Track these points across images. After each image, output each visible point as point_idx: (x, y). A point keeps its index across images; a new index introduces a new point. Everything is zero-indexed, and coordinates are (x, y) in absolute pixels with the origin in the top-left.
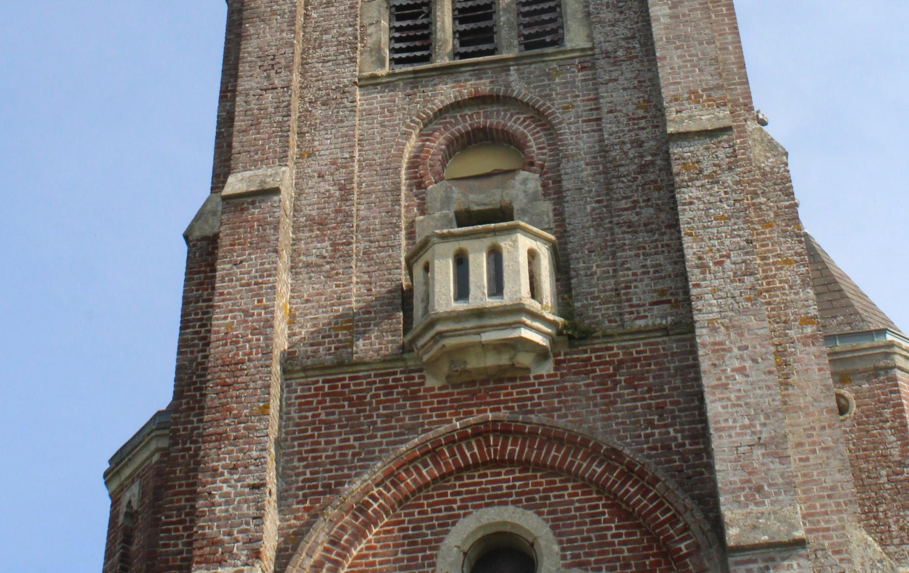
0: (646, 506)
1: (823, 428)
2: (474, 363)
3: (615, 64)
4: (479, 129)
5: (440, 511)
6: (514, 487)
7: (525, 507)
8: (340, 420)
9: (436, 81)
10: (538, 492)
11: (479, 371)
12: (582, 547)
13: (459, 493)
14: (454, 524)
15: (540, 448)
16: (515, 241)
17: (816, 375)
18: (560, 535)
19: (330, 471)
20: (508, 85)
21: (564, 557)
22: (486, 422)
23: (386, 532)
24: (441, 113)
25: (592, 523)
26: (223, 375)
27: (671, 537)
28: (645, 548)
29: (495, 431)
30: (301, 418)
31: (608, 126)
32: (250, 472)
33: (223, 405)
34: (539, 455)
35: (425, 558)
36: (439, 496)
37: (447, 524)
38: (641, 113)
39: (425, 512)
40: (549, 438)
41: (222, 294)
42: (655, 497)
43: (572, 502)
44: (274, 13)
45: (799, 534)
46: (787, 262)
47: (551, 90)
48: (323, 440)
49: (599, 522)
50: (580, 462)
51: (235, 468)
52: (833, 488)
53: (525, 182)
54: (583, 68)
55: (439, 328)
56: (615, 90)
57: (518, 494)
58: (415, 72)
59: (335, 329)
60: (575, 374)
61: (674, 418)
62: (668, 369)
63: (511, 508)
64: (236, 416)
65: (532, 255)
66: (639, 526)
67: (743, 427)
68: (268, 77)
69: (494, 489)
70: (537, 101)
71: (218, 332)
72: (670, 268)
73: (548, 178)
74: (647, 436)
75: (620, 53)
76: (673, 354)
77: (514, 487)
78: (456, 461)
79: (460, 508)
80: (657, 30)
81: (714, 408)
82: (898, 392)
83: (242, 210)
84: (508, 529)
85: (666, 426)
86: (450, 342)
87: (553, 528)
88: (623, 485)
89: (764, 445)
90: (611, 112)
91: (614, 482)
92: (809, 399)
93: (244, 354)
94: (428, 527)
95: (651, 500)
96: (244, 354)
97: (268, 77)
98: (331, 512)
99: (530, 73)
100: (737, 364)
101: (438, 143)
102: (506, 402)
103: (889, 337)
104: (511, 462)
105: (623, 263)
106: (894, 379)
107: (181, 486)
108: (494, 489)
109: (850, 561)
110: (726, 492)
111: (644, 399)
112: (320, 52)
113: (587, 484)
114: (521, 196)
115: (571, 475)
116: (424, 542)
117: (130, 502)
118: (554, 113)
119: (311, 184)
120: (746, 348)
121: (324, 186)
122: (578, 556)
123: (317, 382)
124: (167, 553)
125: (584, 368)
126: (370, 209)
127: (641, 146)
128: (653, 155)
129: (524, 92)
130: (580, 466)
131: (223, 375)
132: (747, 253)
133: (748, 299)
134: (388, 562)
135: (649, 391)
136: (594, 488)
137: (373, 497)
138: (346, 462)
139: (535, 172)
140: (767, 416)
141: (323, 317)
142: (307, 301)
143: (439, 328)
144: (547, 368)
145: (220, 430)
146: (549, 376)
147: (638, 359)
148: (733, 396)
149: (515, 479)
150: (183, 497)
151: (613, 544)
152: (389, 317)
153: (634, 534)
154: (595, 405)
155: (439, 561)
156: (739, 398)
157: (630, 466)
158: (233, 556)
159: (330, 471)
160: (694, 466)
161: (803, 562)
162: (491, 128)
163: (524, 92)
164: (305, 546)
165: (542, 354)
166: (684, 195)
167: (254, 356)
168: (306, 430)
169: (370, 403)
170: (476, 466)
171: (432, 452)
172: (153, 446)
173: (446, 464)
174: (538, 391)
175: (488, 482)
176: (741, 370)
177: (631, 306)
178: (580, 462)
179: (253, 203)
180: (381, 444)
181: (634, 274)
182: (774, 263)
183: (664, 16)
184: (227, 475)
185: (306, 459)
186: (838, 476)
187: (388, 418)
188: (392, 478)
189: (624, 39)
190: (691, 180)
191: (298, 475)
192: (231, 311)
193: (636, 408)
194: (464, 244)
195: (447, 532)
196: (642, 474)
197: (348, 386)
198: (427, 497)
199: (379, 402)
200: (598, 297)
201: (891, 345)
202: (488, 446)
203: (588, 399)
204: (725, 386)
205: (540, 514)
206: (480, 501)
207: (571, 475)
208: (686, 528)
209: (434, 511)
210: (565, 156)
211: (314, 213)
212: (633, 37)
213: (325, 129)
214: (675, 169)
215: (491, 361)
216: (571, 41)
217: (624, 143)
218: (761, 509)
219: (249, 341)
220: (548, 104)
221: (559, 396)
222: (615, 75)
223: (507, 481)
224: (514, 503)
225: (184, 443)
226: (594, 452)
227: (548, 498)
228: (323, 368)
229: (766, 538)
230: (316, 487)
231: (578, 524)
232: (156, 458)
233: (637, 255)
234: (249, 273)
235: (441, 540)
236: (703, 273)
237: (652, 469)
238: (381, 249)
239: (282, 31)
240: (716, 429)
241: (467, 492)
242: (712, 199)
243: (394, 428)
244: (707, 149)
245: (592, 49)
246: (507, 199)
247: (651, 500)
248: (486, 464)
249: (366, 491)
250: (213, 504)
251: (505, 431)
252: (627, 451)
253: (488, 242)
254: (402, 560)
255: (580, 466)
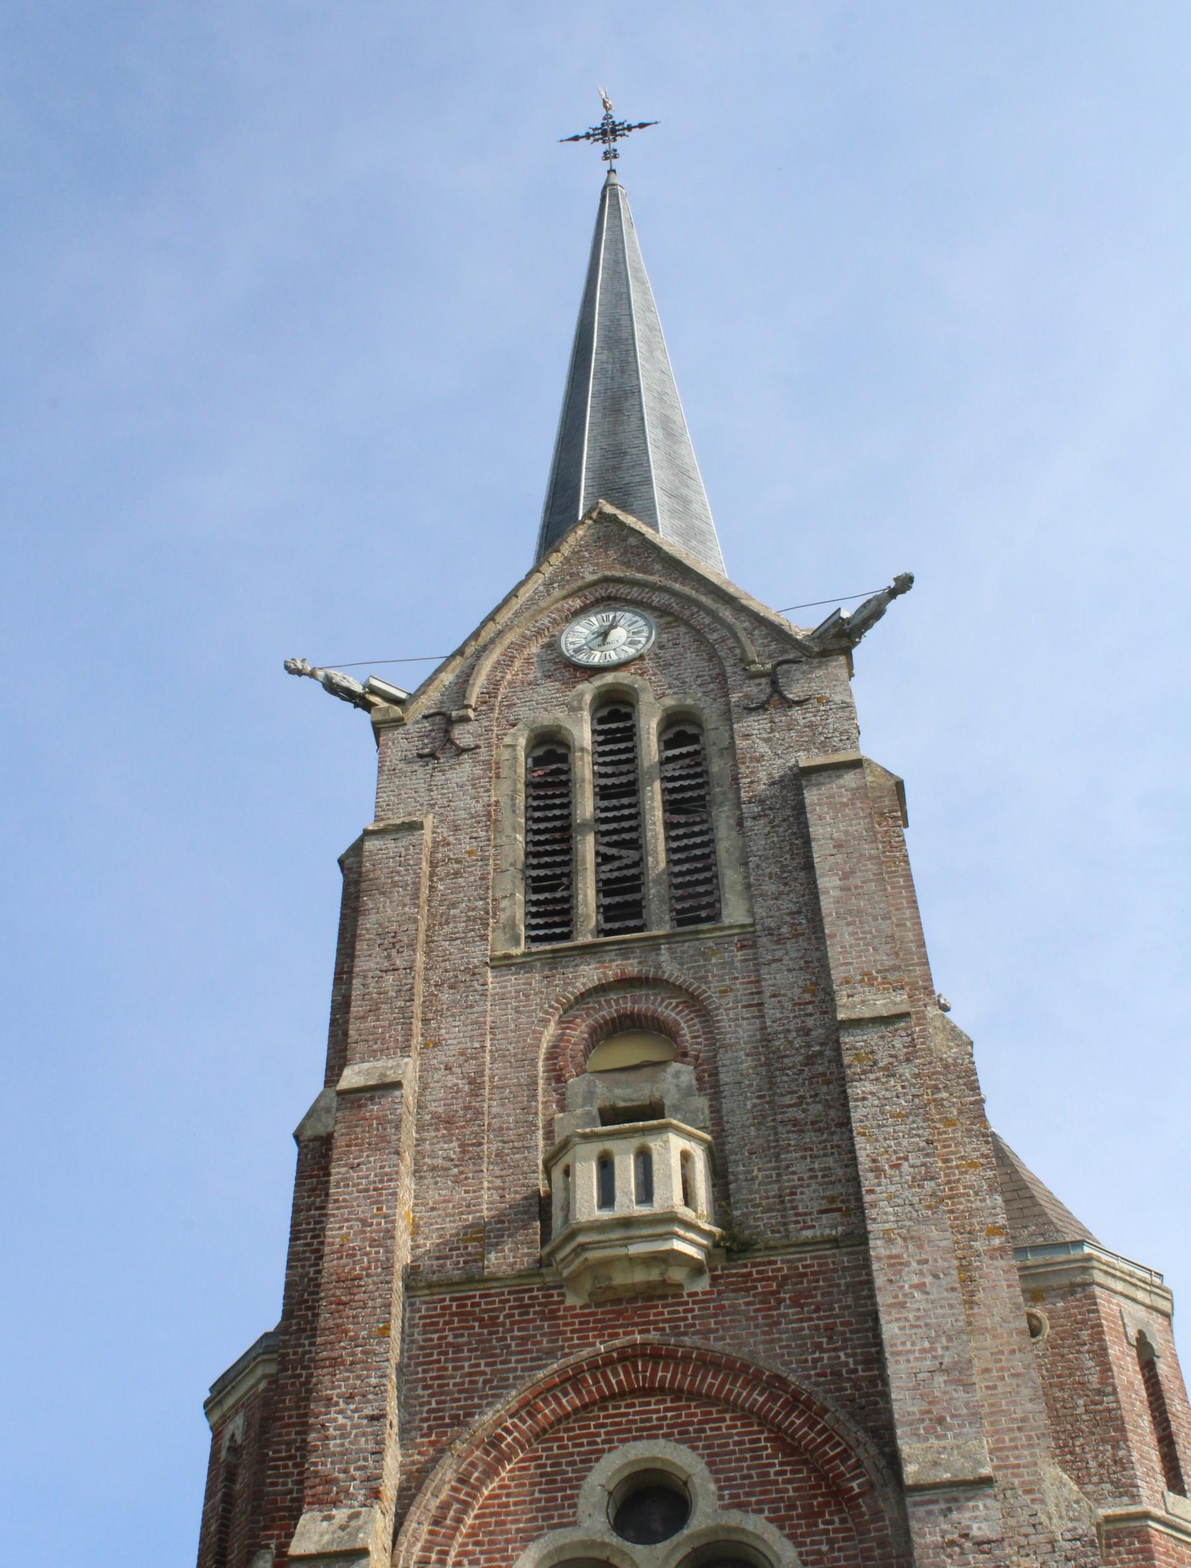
0: (813, 1440)
1: (1013, 1352)
2: (620, 1278)
3: (778, 942)
4: (625, 1016)
5: (582, 1445)
6: (665, 1418)
7: (678, 1441)
8: (469, 1343)
9: (578, 961)
10: (692, 1423)
11: (626, 1288)
12: (741, 1486)
13: (603, 1425)
14: (597, 1460)
15: (694, 1375)
16: (667, 1142)
17: (1005, 1293)
18: (717, 1472)
19: (459, 1400)
20: (658, 966)
21: (721, 1498)
22: (633, 1346)
23: (521, 1469)
24: (583, 997)
25: (753, 1458)
26: (338, 1292)
27: (842, 1474)
28: (812, 1487)
29: (643, 1355)
30: (425, 1340)
31: (771, 1012)
32: (369, 1401)
33: (338, 1326)
34: (692, 1382)
35: (564, 1498)
36: (580, 1428)
37: (590, 1460)
38: (808, 997)
39: (566, 1447)
40: (704, 1363)
41: (336, 1201)
42: (824, 1430)
43: (730, 1436)
44: (395, 884)
45: (986, 1471)
46: (973, 1165)
47: (708, 971)
48: (450, 1365)
49: (760, 1457)
50: (738, 1390)
51: (352, 1396)
52: (1023, 1420)
53: (677, 1075)
54: (743, 947)
55: (581, 1239)
56: (779, 971)
57: (669, 1426)
58: (553, 951)
59: (464, 1241)
60: (733, 1291)
61: (845, 1340)
62: (838, 1285)
63: (662, 1442)
64: (352, 1339)
65: (686, 1157)
66: (805, 1462)
67: (923, 1351)
68: (389, 957)
69: (642, 1421)
70: (691, 984)
71: (332, 1244)
72: (840, 1172)
73: (704, 1071)
74: (815, 1361)
75: (785, 930)
76: (844, 1269)
77: (665, 1418)
78: (599, 1389)
79: (604, 1442)
80: (827, 904)
81: (890, 1329)
82: (1097, 1311)
83: (360, 1106)
84: (659, 1465)
85: (836, 1349)
86: (594, 1255)
87: (709, 1464)
88: (787, 1415)
89: (946, 1371)
90: (774, 996)
91: (778, 1413)
92: (997, 1319)
93: (362, 1269)
94: (569, 1464)
95: (819, 1433)
96: (362, 1269)
97: (389, 957)
98: (459, 1446)
99: (683, 952)
100: (916, 1280)
101: (580, 1031)
102: (656, 1322)
103: (1087, 1250)
104: (662, 1389)
105: (788, 1167)
106: (1093, 1297)
107: (290, 1417)
108: (642, 1421)
109: (1042, 1501)
110: (904, 1424)
111: (811, 1319)
112: (446, 929)
113: (747, 1415)
114: (673, 1090)
115: (730, 1405)
116: (564, 1481)
117: (233, 1435)
118: (710, 997)
119: (436, 1077)
120: (926, 1261)
121: (451, 1080)
122: (737, 1496)
123: (444, 1300)
124: (275, 1493)
125: (744, 1285)
126: (503, 1105)
127: (807, 1034)
128: (821, 1044)
129: (676, 973)
130: (739, 1394)
131: (338, 1292)
132: (927, 1155)
133: (929, 1207)
134: (524, 1502)
135: (817, 1310)
136: (754, 1420)
137: (506, 1430)
138: (476, 1390)
139: (689, 1064)
140: (950, 1339)
141: (451, 1227)
142: (433, 1209)
143: (581, 1239)
144: (703, 1285)
145: (335, 1354)
146: (704, 1293)
147: (805, 1275)
148: (911, 1316)
149: (667, 1410)
150: (293, 1430)
151: (776, 1482)
152: (525, 1227)
153: (800, 1471)
154: (756, 1326)
155: (581, 1502)
156: (918, 1318)
157: (796, 1395)
158: (349, 1495)
159: (459, 1400)
160: (867, 1395)
161: (990, 1502)
162: (639, 1015)
163: (676, 973)
164: (430, 1485)
165: (697, 1269)
166: (856, 1090)
167: (372, 1271)
168: (431, 1355)
169: (504, 1324)
170: (622, 1394)
171: (572, 1379)
172: (259, 1372)
173: (589, 1392)
174: (692, 1310)
175: (636, 1413)
176: (921, 1287)
177: (797, 1215)
178: (738, 1390)
179: (372, 1099)
180: (515, 1369)
181: (801, 1179)
182: (958, 1167)
183: (834, 888)
184: (342, 1405)
185: (431, 1387)
186: (1029, 1406)
187: (523, 1340)
188: (528, 1408)
189: (789, 914)
190: (864, 1072)
191: (422, 1404)
192: (347, 1220)
193: (802, 1329)
194: (609, 1145)
195: (590, 1469)
196: (809, 1404)
197: (478, 1304)
198: (567, 1430)
199: (513, 1323)
200: (760, 1205)
201: (1089, 1258)
202: (636, 1372)
203: (748, 1319)
204: (902, 1305)
205: (694, 1448)
206: (627, 1434)
207: (730, 1405)
208: (859, 1464)
209: (574, 1446)
210: (723, 1046)
211: (440, 1110)
212: (799, 912)
213: (453, 1015)
214: (847, 1060)
215: (640, 1276)
216: (730, 916)
217: (788, 1031)
218: (943, 1443)
219: (367, 1254)
220: (704, 987)
221: (715, 1315)
222: (778, 954)
223: (658, 1411)
224: (665, 1436)
225: (294, 1369)
226: (755, 1379)
227: (703, 1430)
228: (450, 1284)
229: (949, 1475)
230: (443, 1418)
231: (737, 1460)
232: (262, 1385)
233: (804, 1158)
234: (367, 1177)
235: (583, 1478)
236: (878, 1177)
237: (821, 1398)
238: (517, 1150)
239: (405, 905)
240: (893, 1353)
241: (613, 1424)
242: (888, 1094)
243: (531, 1351)
244: (882, 1037)
245: (753, 925)
246: (657, 1094)
247: (819, 1433)
248: (633, 1392)
249: (499, 1423)
250: (327, 1438)
251: (656, 1355)
252: (792, 1378)
253: (635, 1142)
254: (539, 1500)
255: (739, 1394)
